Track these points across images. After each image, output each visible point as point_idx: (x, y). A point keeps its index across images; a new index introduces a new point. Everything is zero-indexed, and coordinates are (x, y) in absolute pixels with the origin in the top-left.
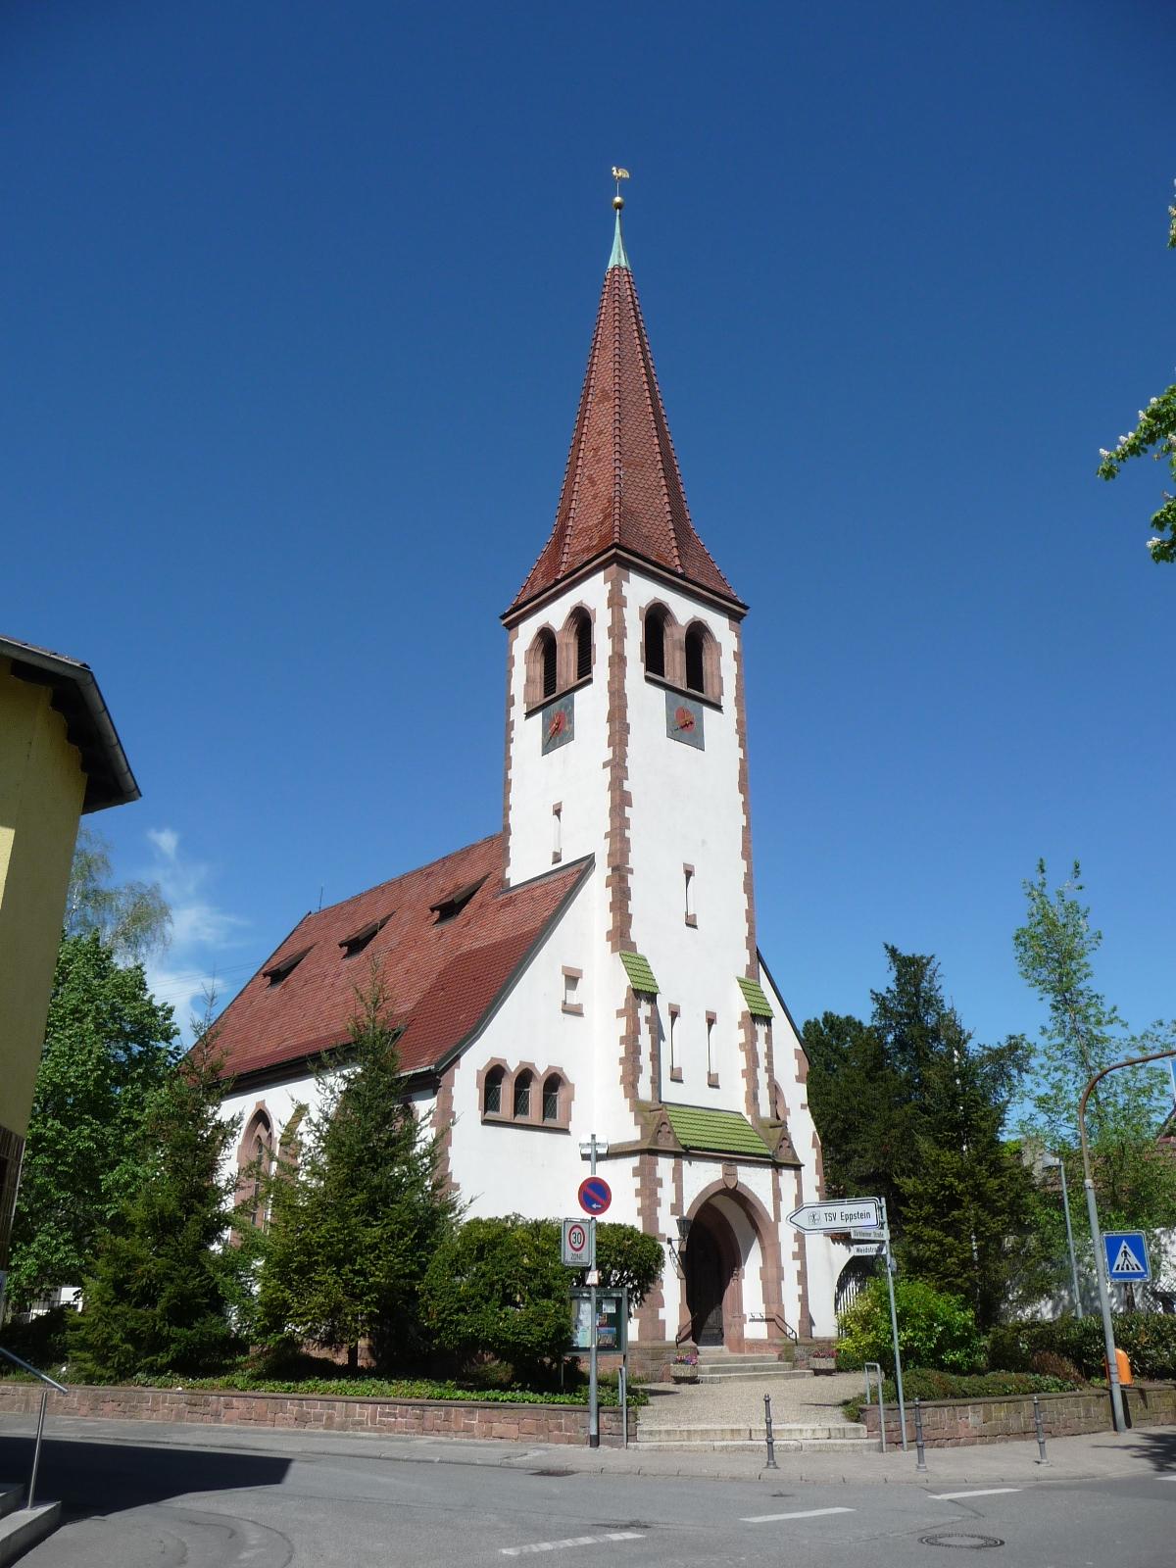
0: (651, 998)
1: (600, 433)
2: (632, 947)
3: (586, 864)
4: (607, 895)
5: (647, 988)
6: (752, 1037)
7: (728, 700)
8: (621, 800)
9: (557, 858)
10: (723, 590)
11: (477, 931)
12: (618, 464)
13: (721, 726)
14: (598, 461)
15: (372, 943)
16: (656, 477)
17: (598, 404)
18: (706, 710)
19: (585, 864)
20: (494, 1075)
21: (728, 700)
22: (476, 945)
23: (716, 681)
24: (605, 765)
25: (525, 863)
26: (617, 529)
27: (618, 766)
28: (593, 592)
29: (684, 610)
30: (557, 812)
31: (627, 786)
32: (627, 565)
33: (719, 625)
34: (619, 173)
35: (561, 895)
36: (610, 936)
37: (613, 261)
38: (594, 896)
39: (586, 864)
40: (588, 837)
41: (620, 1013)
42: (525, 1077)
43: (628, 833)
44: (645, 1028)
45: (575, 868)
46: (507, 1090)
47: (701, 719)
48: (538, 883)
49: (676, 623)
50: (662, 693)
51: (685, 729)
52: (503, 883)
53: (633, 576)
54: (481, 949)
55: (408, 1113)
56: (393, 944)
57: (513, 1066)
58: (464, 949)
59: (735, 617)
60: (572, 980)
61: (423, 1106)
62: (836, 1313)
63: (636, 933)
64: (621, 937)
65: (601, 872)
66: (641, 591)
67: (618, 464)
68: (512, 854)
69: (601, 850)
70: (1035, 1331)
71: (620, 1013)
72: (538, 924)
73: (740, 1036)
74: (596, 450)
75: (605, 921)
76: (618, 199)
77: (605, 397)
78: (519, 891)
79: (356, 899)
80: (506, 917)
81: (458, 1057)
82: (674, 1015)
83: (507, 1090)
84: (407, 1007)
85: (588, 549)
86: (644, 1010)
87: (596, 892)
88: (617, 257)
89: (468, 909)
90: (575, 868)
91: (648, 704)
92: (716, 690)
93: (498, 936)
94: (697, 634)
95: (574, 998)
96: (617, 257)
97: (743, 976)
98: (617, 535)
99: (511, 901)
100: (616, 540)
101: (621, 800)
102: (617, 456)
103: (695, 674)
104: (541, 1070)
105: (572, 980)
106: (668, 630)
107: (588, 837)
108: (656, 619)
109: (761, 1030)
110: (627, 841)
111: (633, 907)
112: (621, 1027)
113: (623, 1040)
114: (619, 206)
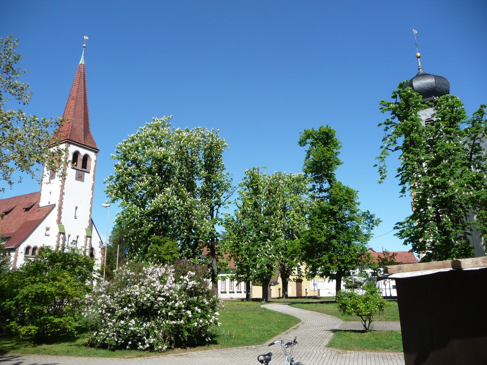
0: (64, 234)
1: (71, 108)
2: (61, 223)
3: (54, 205)
4: (57, 213)
5: (62, 232)
6: (87, 240)
7: (92, 171)
8: (62, 194)
9: (49, 203)
10: (94, 146)
11: (32, 216)
12: (73, 117)
13: (89, 177)
14: (69, 115)
15: (10, 213)
16: (82, 120)
17: (71, 100)
18: (86, 173)
19: (54, 205)
20: (28, 248)
21: (92, 171)
22: (30, 220)
23: (89, 167)
24: (60, 186)
25: (43, 203)
26: (69, 135)
27: (62, 187)
28: (63, 146)
29: (83, 152)
30: (50, 193)
31: (64, 191)
32: (70, 143)
33: (92, 154)
34: (86, 38)
35: (48, 212)
36: (57, 221)
37: (81, 62)
38: (54, 213)
39: (54, 205)
40: (55, 200)
41: (57, 236)
42: (35, 248)
43: (63, 201)
44: (61, 239)
45: (51, 206)
46: (31, 251)
47: (84, 176)
48: (45, 208)
49: (81, 155)
50: (75, 171)
51: (80, 178)
52: (39, 205)
53: (71, 146)
54: (31, 221)
55: (9, 255)
56: (15, 214)
57: (32, 246)
58: (28, 220)
59: (96, 152)
60: (48, 229)
61: (13, 254)
62: (413, 211)
63: (62, 221)
64: (59, 221)
65: (57, 208)
66: (73, 149)
67: (73, 117)
68: (41, 200)
69: (57, 203)
70: (310, 260)
71: (57, 236)
72: (42, 218)
73: (84, 240)
74: (69, 112)
75: (56, 218)
76: (84, 45)
77: (73, 99)
78: (41, 208)
79: (10, 199)
80: (37, 214)
81: (20, 245)
82: (69, 236)
83: (31, 251)
84: (14, 231)
85: (63, 136)
86: (62, 236)
87: (55, 212)
88: (82, 61)
89: (31, 210)
90: (51, 206)
91: (71, 173)
92: (89, 169)
93: (34, 219)
94: (86, 157)
95: (48, 233)
96: (82, 61)
97: (87, 228)
98: (69, 136)
99: (39, 211)
100: (68, 138)
101: (62, 194)
102: (73, 115)
103: (84, 165)
104: (39, 247)
105: (48, 229)
106: (79, 156)
107: (55, 200)
108: (76, 155)
109: (89, 239)
110: (62, 202)
111: (62, 215)
112: (56, 239)
113: (56, 241)
114: (84, 47)
